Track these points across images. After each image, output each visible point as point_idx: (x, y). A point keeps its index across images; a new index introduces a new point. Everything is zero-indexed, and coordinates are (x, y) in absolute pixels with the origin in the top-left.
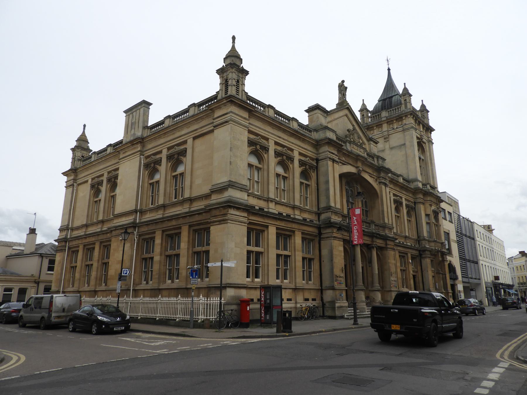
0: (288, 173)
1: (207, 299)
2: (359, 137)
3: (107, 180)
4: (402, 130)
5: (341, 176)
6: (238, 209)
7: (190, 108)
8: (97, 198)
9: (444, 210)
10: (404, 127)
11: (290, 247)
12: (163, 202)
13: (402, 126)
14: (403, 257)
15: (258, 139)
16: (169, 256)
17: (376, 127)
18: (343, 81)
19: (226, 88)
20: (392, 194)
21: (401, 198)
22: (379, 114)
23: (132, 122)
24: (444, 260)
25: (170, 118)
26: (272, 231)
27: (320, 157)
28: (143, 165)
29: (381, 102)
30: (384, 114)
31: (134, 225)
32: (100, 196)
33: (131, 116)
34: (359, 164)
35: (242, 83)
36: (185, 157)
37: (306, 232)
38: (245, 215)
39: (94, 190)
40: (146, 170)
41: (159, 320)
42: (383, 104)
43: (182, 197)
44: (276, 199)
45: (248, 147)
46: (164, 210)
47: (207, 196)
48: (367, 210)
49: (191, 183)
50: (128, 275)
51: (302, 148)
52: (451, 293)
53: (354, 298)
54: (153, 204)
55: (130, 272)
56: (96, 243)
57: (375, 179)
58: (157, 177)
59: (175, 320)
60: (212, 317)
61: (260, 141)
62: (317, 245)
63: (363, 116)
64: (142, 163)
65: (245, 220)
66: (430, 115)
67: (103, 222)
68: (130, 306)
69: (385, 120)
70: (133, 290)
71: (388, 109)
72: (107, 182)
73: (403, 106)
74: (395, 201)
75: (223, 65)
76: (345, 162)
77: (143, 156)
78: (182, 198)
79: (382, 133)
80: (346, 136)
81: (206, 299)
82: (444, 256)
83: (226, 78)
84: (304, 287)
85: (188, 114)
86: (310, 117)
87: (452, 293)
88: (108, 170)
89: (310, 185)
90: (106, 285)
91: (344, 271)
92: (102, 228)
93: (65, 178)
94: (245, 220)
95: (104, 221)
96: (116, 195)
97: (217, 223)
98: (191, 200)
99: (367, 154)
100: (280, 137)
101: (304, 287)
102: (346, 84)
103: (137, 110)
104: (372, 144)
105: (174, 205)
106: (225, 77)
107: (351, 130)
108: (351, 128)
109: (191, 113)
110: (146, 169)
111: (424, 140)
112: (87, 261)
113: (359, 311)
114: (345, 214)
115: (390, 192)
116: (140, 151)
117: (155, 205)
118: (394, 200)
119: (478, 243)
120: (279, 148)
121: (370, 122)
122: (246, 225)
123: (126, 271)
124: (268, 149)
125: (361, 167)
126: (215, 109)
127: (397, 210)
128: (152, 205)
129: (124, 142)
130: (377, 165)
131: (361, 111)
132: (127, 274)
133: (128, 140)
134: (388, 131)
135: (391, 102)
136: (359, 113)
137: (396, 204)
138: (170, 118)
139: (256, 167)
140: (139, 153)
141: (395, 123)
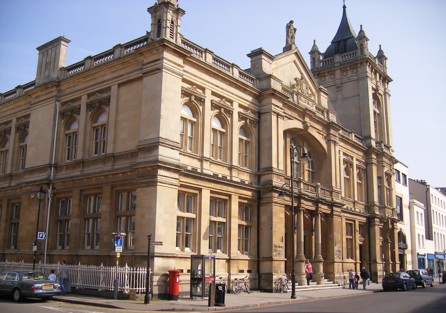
0: (225, 128)
1: (133, 269)
2: (308, 88)
3: (16, 128)
4: (356, 79)
5: (286, 132)
6: (168, 169)
9: (398, 172)
10: (359, 75)
11: (226, 213)
12: (82, 158)
13: (356, 74)
14: (351, 224)
15: (193, 88)
17: (328, 74)
18: (292, 22)
19: (158, 30)
20: (341, 153)
21: (352, 158)
22: (332, 58)
24: (393, 228)
28: (59, 113)
29: (334, 44)
30: (338, 58)
31: (49, 183)
32: (7, 145)
33: (46, 53)
35: (177, 24)
37: (244, 196)
38: (176, 176)
40: (62, 119)
41: (79, 289)
42: (337, 47)
43: (103, 152)
44: (212, 158)
45: (181, 97)
46: (83, 167)
49: (115, 136)
50: (44, 238)
51: (243, 99)
52: (399, 264)
53: (293, 271)
54: (70, 159)
57: (324, 136)
58: (75, 127)
59: (97, 290)
60: (139, 287)
61: (196, 92)
62: (256, 211)
63: (313, 60)
64: (58, 110)
65: (176, 182)
66: (388, 63)
67: (11, 176)
70: (47, 255)
71: (342, 53)
72: (16, 130)
73: (359, 51)
74: (345, 162)
75: (156, 3)
76: (291, 116)
77: (59, 102)
78: (104, 154)
79: (335, 81)
80: (293, 86)
81: (132, 269)
82: (395, 224)
83: (158, 18)
84: (239, 257)
87: (400, 264)
88: (18, 116)
90: (16, 248)
91: (284, 241)
92: (10, 183)
94: (176, 182)
95: (13, 175)
97: (145, 185)
98: (114, 157)
99: (316, 107)
101: (239, 257)
102: (295, 25)
104: (322, 95)
105: (95, 162)
106: (158, 17)
107: (299, 79)
108: (299, 76)
109: (117, 53)
111: (380, 91)
113: (297, 284)
115: (339, 151)
116: (55, 96)
117: (71, 160)
118: (344, 160)
119: (432, 209)
120: (217, 99)
121: (321, 67)
122: (177, 187)
123: (42, 235)
124: (204, 100)
125: (309, 122)
126: (145, 53)
127: (347, 171)
128: (68, 159)
129: (36, 84)
131: (312, 54)
132: (42, 238)
133: (41, 82)
134: (341, 79)
135: (345, 46)
136: (310, 55)
137: (346, 165)
138: (92, 60)
140: (54, 98)
141: (349, 70)
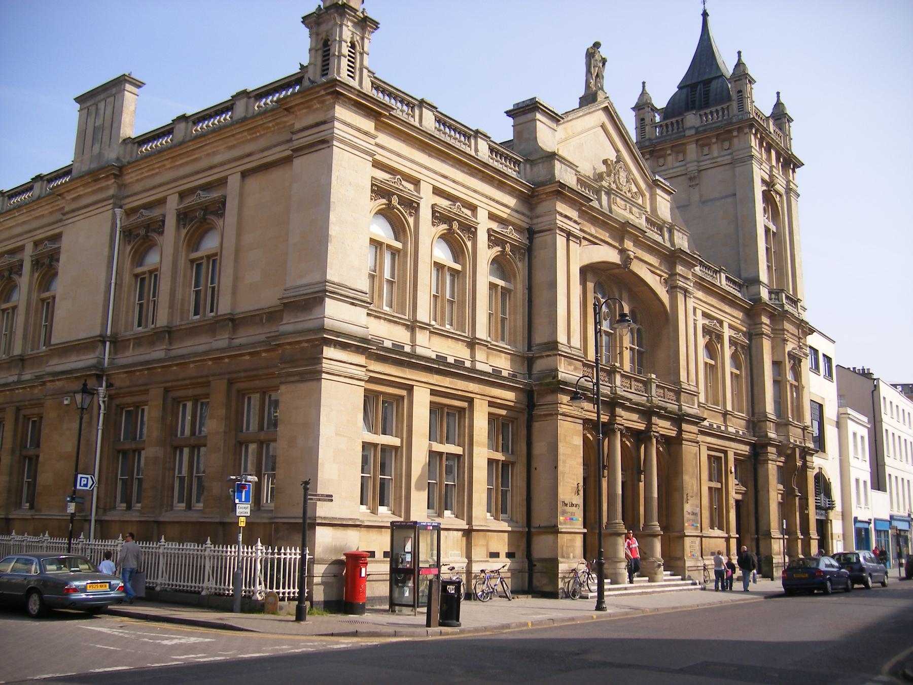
0: (461, 262)
1: (273, 549)
2: (630, 179)
3: (32, 261)
5: (585, 271)
6: (344, 346)
8: (8, 302)
9: (816, 352)
10: (734, 154)
12: (168, 322)
13: (729, 151)
15: (396, 181)
17: (672, 150)
18: (597, 45)
19: (324, 61)
20: (699, 313)
21: (721, 322)
22: (679, 118)
23: (96, 124)
24: (805, 467)
26: (422, 400)
27: (537, 224)
28: (120, 231)
29: (685, 91)
30: (692, 119)
32: (15, 297)
33: (93, 108)
34: (629, 244)
35: (363, 49)
36: (221, 217)
37: (499, 401)
38: (361, 359)
40: (127, 242)
41: (161, 591)
43: (212, 311)
44: (433, 323)
45: (372, 199)
47: (272, 315)
48: (642, 349)
49: (236, 278)
50: (90, 488)
51: (497, 202)
52: (816, 539)
54: (143, 324)
55: (93, 483)
57: (663, 278)
58: (152, 259)
59: (199, 593)
60: (284, 588)
61: (401, 187)
62: (524, 432)
64: (118, 226)
65: (360, 373)
67: (22, 361)
68: (91, 556)
69: (692, 135)
70: (96, 521)
71: (700, 108)
72: (33, 266)
73: (735, 105)
74: (706, 331)
75: (320, 6)
76: (596, 238)
79: (685, 165)
80: (600, 177)
81: (270, 551)
82: (808, 458)
83: (324, 37)
84: (489, 527)
86: (518, 127)
87: (818, 540)
89: (512, 290)
90: (32, 507)
91: (581, 492)
92: (20, 375)
94: (359, 373)
95: (26, 357)
97: (296, 378)
98: (234, 322)
99: (647, 220)
100: (446, 177)
101: (489, 527)
102: (603, 52)
103: (108, 97)
105: (193, 331)
106: (324, 35)
107: (612, 161)
108: (613, 156)
109: (240, 109)
110: (127, 239)
111: (778, 187)
113: (609, 581)
114: (589, 361)
115: (695, 309)
116: (113, 196)
117: (146, 327)
118: (704, 327)
119: (885, 427)
120: (444, 203)
121: (657, 138)
122: (362, 383)
123: (86, 480)
124: (418, 204)
126: (296, 108)
127: (711, 350)
128: (139, 325)
130: (668, 245)
131: (639, 110)
132: (87, 487)
133: (85, 168)
134: (699, 162)
135: (707, 94)
136: (633, 113)
139: (389, 247)
140: (111, 201)
141: (714, 143)
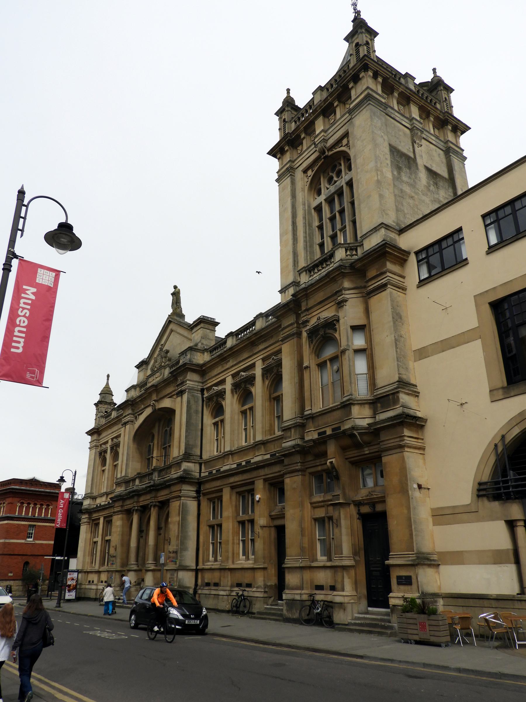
7: (257, 319)
16: (242, 523)
25: (263, 317)
39: (211, 406)
56: (224, 490)
85: (254, 327)
93: (89, 438)
96: (282, 395)
112: (95, 538)
